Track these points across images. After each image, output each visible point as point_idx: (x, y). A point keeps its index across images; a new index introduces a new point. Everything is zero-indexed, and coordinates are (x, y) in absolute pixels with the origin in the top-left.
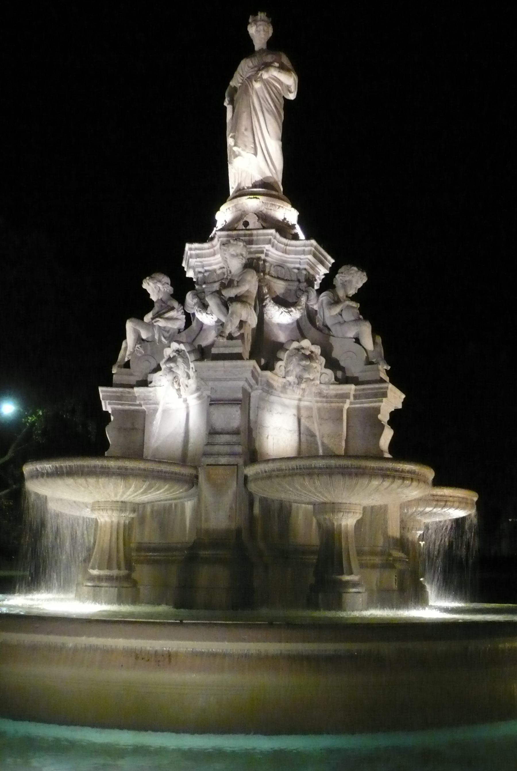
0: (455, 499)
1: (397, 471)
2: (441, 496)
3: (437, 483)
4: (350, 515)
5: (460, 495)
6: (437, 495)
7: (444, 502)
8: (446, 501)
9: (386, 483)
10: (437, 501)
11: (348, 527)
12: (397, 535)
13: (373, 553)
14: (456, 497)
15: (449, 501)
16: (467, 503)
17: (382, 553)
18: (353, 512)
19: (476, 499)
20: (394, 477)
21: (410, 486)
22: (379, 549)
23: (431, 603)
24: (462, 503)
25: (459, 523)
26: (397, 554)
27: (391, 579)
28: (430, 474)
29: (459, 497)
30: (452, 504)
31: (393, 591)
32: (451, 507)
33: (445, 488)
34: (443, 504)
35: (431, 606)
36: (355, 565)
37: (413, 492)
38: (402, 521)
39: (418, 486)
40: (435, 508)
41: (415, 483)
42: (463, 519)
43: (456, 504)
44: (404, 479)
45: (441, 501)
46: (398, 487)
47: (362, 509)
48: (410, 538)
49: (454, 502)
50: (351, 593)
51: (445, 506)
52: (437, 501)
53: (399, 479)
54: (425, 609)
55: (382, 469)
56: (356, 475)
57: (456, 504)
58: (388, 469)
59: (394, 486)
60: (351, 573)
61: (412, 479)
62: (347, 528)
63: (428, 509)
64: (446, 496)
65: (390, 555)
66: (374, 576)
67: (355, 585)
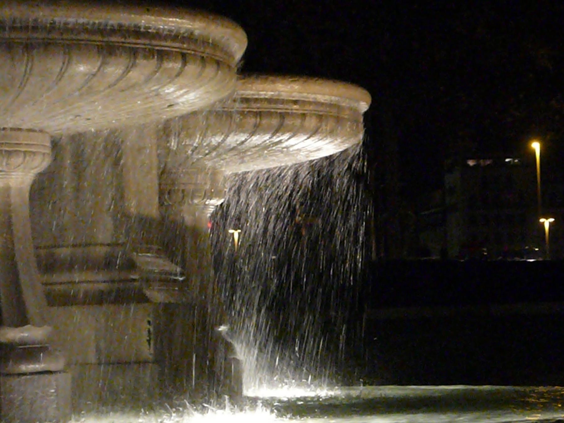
0: (307, 107)
1: (137, 32)
2: (270, 101)
3: (255, 65)
4: (17, 160)
5: (321, 98)
6: (256, 100)
7: (280, 118)
8: (283, 116)
9: (114, 70)
10: (259, 114)
11: (13, 192)
12: (153, 211)
13: (89, 265)
14: (310, 103)
15: (292, 115)
16: (338, 120)
17: (108, 264)
18: (25, 153)
19: (364, 107)
20: (134, 53)
21: (178, 75)
22: (101, 251)
23: (249, 391)
24: (324, 120)
25: (323, 170)
26: (151, 262)
27: (137, 331)
28: (235, 42)
29: (317, 103)
30: (298, 122)
31: (141, 363)
32: (295, 132)
33: (279, 78)
34: (275, 122)
35: (254, 400)
36: (33, 300)
37: (188, 94)
38: (163, 173)
39: (200, 75)
40: (252, 134)
41: (192, 68)
42: (330, 159)
43: (311, 122)
44: (162, 55)
45: (270, 114)
46: (148, 80)
47: (48, 144)
48: (188, 219)
49: (304, 115)
50: (24, 374)
51: (277, 130)
52: (259, 114)
53: (146, 57)
54: (385, 395)
55: (102, 30)
56: (28, 47)
57: (311, 122)
58: (120, 30)
59: (135, 75)
60: (22, 320)
61: (184, 57)
62: (9, 196)
63: (234, 139)
64: (283, 102)
65: (131, 265)
66: (86, 326)
67: (30, 352)
